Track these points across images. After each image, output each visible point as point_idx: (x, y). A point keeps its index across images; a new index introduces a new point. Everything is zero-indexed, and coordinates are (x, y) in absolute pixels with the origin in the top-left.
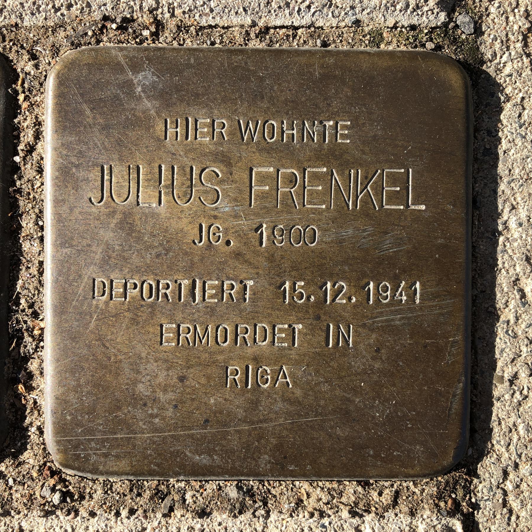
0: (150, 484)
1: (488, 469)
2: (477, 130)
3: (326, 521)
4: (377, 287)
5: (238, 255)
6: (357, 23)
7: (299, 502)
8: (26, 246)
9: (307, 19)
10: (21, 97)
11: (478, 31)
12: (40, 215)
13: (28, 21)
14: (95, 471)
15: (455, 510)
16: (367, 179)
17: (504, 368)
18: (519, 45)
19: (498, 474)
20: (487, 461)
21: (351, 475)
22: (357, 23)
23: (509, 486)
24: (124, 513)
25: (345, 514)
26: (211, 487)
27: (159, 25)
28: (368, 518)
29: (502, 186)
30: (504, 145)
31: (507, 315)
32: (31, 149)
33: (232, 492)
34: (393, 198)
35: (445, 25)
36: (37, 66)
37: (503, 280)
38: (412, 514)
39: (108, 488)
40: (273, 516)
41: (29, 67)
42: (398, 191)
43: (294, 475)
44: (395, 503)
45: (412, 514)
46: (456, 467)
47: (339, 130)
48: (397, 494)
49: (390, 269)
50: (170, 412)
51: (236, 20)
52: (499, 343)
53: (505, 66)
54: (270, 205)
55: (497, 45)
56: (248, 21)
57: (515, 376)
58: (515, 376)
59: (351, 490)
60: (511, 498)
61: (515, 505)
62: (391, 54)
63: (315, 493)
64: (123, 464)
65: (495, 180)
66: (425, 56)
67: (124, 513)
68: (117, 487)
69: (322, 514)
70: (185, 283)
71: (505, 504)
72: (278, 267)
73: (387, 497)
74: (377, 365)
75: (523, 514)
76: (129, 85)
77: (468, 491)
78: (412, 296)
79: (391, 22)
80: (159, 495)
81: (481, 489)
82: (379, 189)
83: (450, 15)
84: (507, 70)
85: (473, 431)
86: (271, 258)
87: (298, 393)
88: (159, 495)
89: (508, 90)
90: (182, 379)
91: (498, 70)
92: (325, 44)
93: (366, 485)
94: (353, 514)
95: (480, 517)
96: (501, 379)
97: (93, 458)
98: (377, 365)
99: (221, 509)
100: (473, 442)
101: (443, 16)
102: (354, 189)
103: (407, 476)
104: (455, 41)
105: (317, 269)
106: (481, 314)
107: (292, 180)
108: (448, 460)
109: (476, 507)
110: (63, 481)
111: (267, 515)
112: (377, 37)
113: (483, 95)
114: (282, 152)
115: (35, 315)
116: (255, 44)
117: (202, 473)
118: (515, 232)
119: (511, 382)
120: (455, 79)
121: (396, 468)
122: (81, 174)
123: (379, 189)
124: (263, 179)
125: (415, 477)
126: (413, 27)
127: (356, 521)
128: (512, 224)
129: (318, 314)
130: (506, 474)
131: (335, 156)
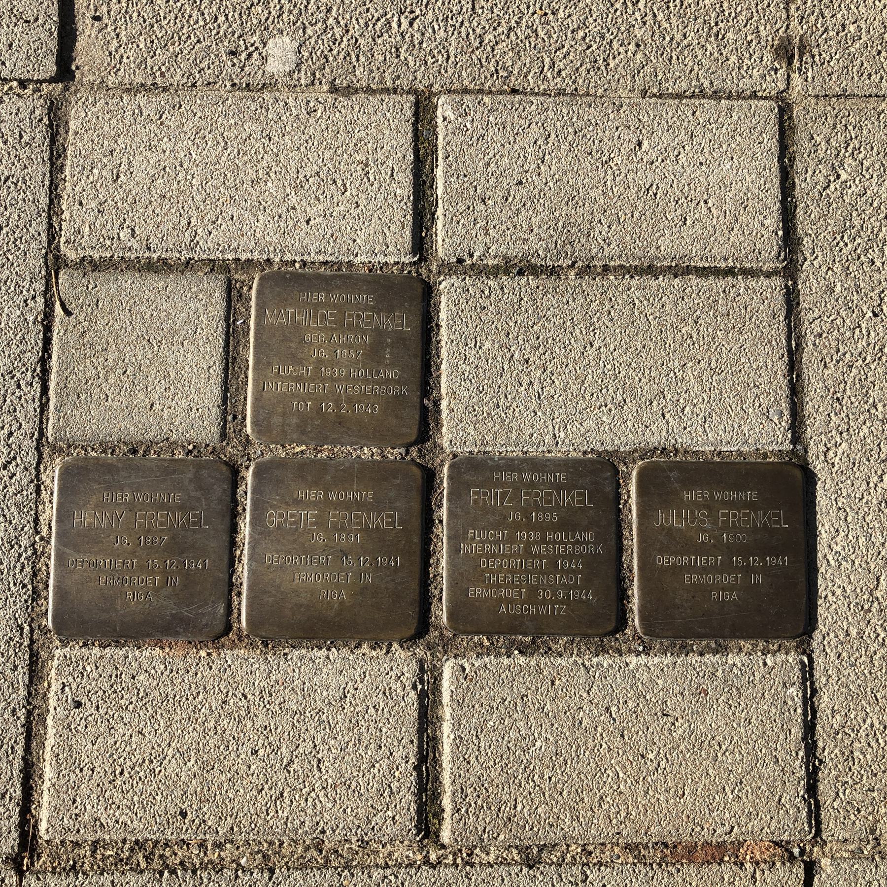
0: (679, 642)
1: (817, 635)
2: (807, 493)
3: (751, 657)
4: (562, 562)
5: (715, 546)
6: (757, 449)
7: (740, 649)
8: (625, 542)
9: (737, 448)
10: (621, 481)
11: (806, 452)
12: (631, 530)
13: (622, 449)
14: (658, 637)
15: (804, 653)
16: (765, 515)
17: (821, 592)
18: (823, 457)
19: (821, 637)
20: (817, 632)
21: (761, 638)
22: (757, 449)
23: (826, 643)
24: (669, 655)
25: (759, 654)
26: (704, 643)
27: (676, 450)
28: (769, 656)
29: (818, 516)
30: (818, 499)
31: (822, 570)
32: (626, 502)
33: (713, 645)
34: (776, 522)
35: (793, 449)
36: (627, 468)
37: (820, 555)
38: (787, 654)
39: (661, 644)
40: (730, 655)
41: (624, 468)
42: (780, 521)
43: (739, 638)
44: (779, 650)
45: (787, 654)
46: (804, 634)
47: (751, 495)
48: (780, 646)
49: (775, 552)
50: (689, 611)
51: (708, 449)
52: (819, 582)
53: (818, 466)
54: (725, 527)
55: (814, 457)
56: (713, 449)
57: (827, 596)
58: (827, 596)
59: (761, 644)
60: (827, 647)
61: (828, 651)
62: (772, 463)
63: (747, 645)
64: (670, 633)
65: (815, 513)
66: (786, 463)
67: (669, 655)
68: (665, 643)
69: (750, 654)
70: (519, 561)
71: (824, 650)
72: (730, 550)
73: (776, 647)
74: (771, 591)
75: (832, 654)
76: (669, 477)
77: (809, 645)
78: (784, 562)
79: (771, 449)
80: (683, 647)
81: (815, 644)
82: (769, 519)
83: (795, 447)
84: (818, 468)
85: (810, 619)
86: (728, 548)
87: (740, 602)
88: (683, 647)
89: (819, 476)
90: (693, 597)
91: (815, 468)
92: (745, 459)
93: (767, 642)
94: (763, 654)
95: (814, 655)
96: (821, 597)
97: (657, 631)
98: (771, 591)
99: (709, 653)
100: (810, 624)
101: (792, 447)
102: (760, 519)
103: (785, 638)
104: (797, 456)
105: (745, 551)
106: (812, 570)
107: (735, 515)
108: (801, 631)
109: (812, 651)
110: (643, 641)
111: (727, 656)
112: (765, 455)
113: (810, 478)
114: (731, 504)
115: (631, 571)
116: (716, 459)
117: (701, 637)
118: (824, 535)
119: (825, 599)
120: (798, 473)
121: (778, 635)
122: (650, 513)
123: (769, 519)
124: (723, 515)
125: (787, 638)
126: (780, 451)
127: (763, 657)
128: (823, 532)
129: (747, 570)
130: (824, 638)
131: (751, 505)
